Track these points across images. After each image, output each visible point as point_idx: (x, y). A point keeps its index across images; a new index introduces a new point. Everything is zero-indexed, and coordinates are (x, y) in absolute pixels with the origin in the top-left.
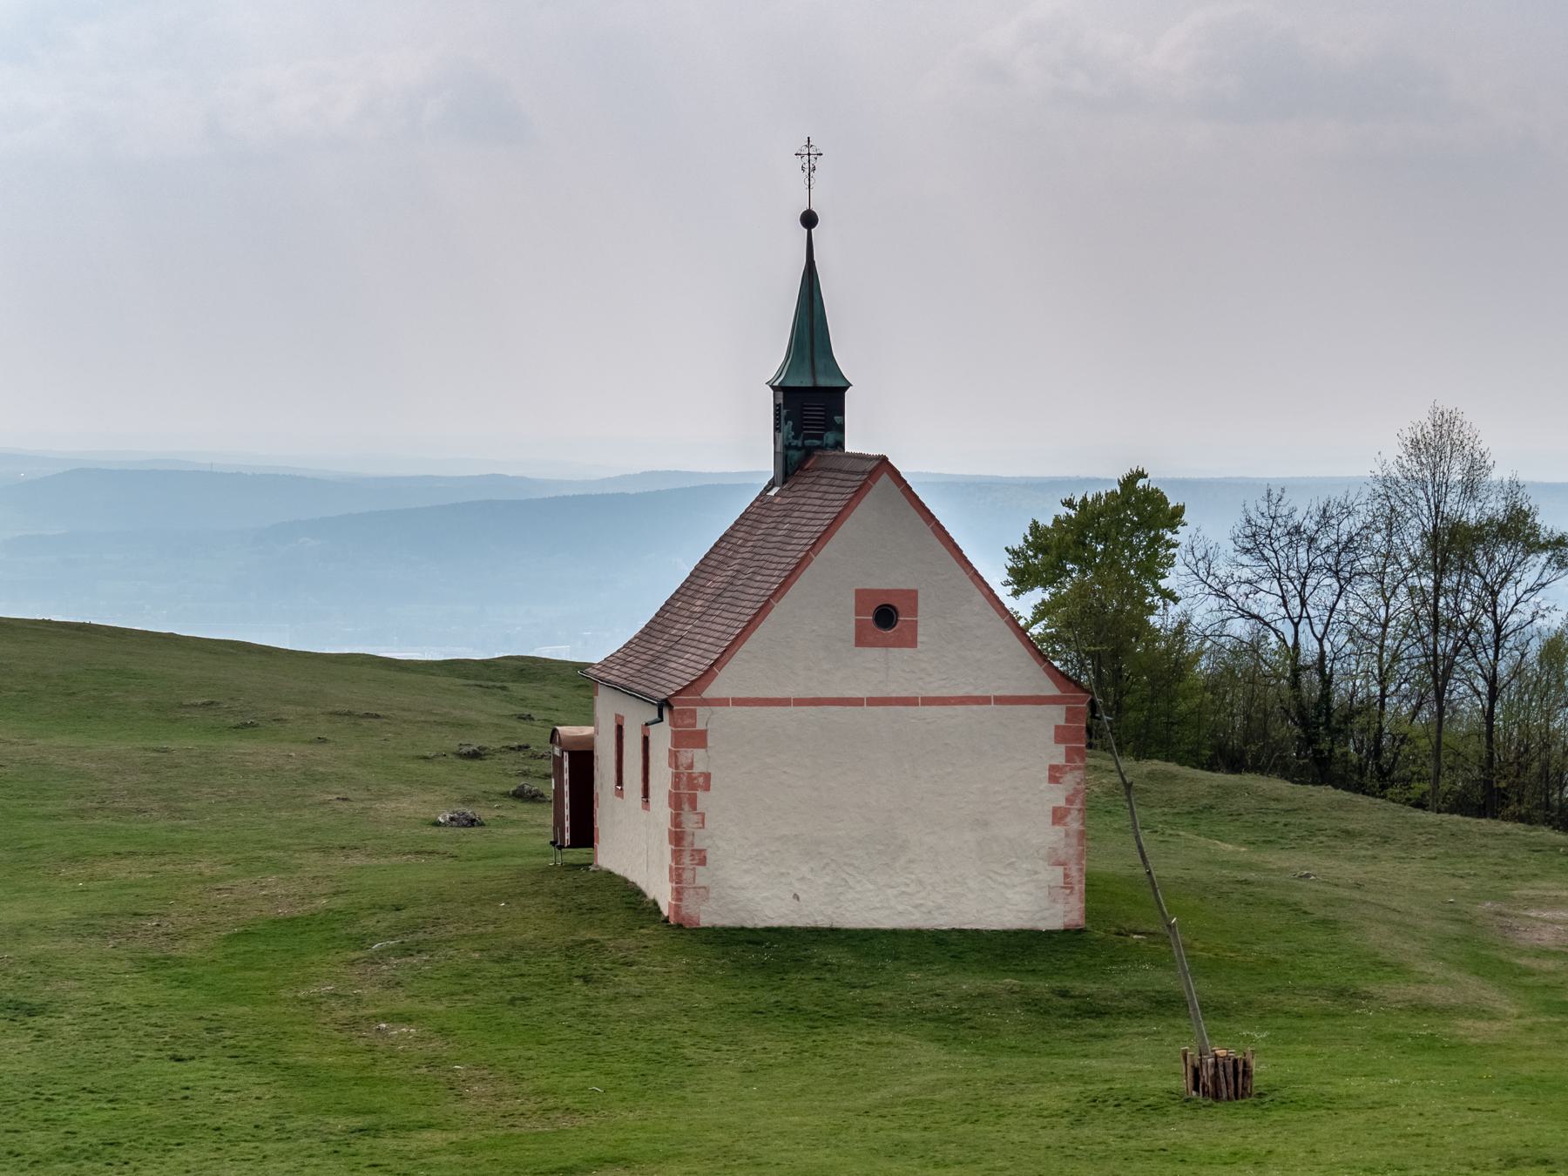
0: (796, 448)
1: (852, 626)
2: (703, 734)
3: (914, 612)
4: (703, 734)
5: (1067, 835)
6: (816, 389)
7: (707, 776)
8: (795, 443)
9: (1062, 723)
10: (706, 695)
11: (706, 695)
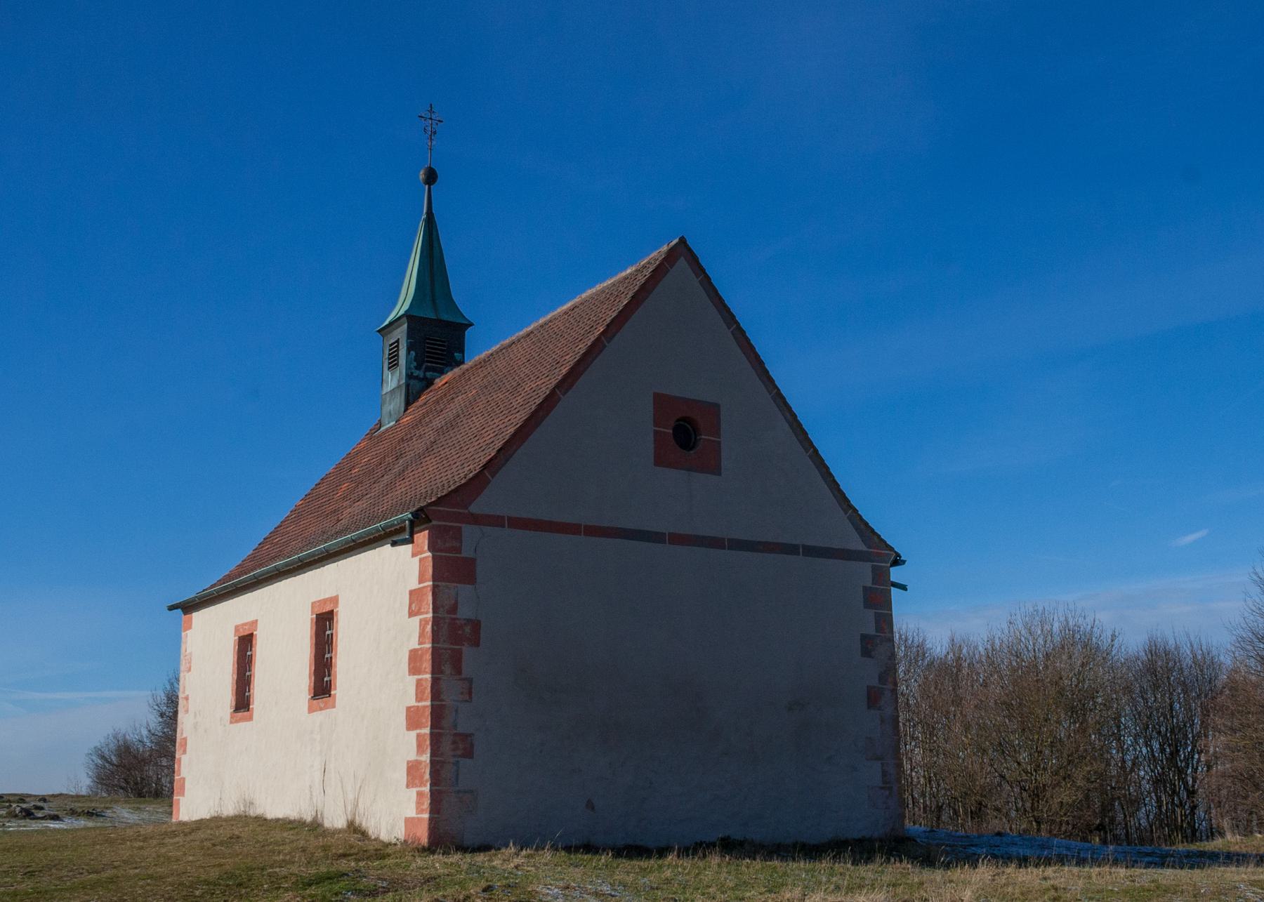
0: (417, 378)
1: (651, 438)
2: (471, 562)
3: (716, 431)
4: (471, 562)
5: (882, 721)
6: (440, 322)
7: (476, 625)
8: (416, 373)
9: (413, 703)
10: (474, 508)
11: (474, 508)
